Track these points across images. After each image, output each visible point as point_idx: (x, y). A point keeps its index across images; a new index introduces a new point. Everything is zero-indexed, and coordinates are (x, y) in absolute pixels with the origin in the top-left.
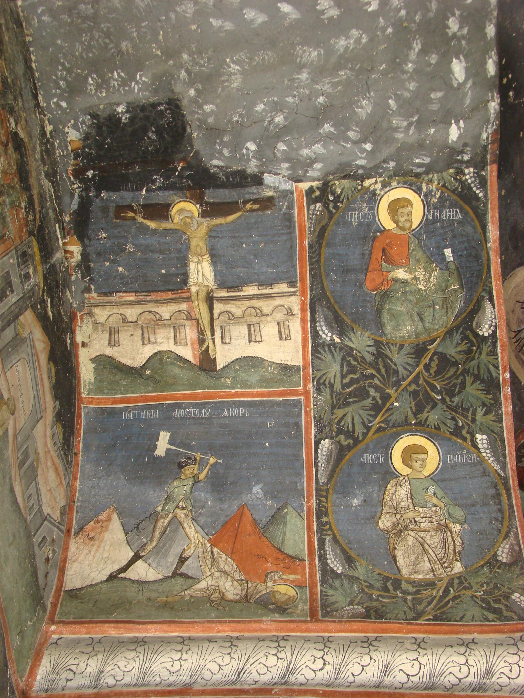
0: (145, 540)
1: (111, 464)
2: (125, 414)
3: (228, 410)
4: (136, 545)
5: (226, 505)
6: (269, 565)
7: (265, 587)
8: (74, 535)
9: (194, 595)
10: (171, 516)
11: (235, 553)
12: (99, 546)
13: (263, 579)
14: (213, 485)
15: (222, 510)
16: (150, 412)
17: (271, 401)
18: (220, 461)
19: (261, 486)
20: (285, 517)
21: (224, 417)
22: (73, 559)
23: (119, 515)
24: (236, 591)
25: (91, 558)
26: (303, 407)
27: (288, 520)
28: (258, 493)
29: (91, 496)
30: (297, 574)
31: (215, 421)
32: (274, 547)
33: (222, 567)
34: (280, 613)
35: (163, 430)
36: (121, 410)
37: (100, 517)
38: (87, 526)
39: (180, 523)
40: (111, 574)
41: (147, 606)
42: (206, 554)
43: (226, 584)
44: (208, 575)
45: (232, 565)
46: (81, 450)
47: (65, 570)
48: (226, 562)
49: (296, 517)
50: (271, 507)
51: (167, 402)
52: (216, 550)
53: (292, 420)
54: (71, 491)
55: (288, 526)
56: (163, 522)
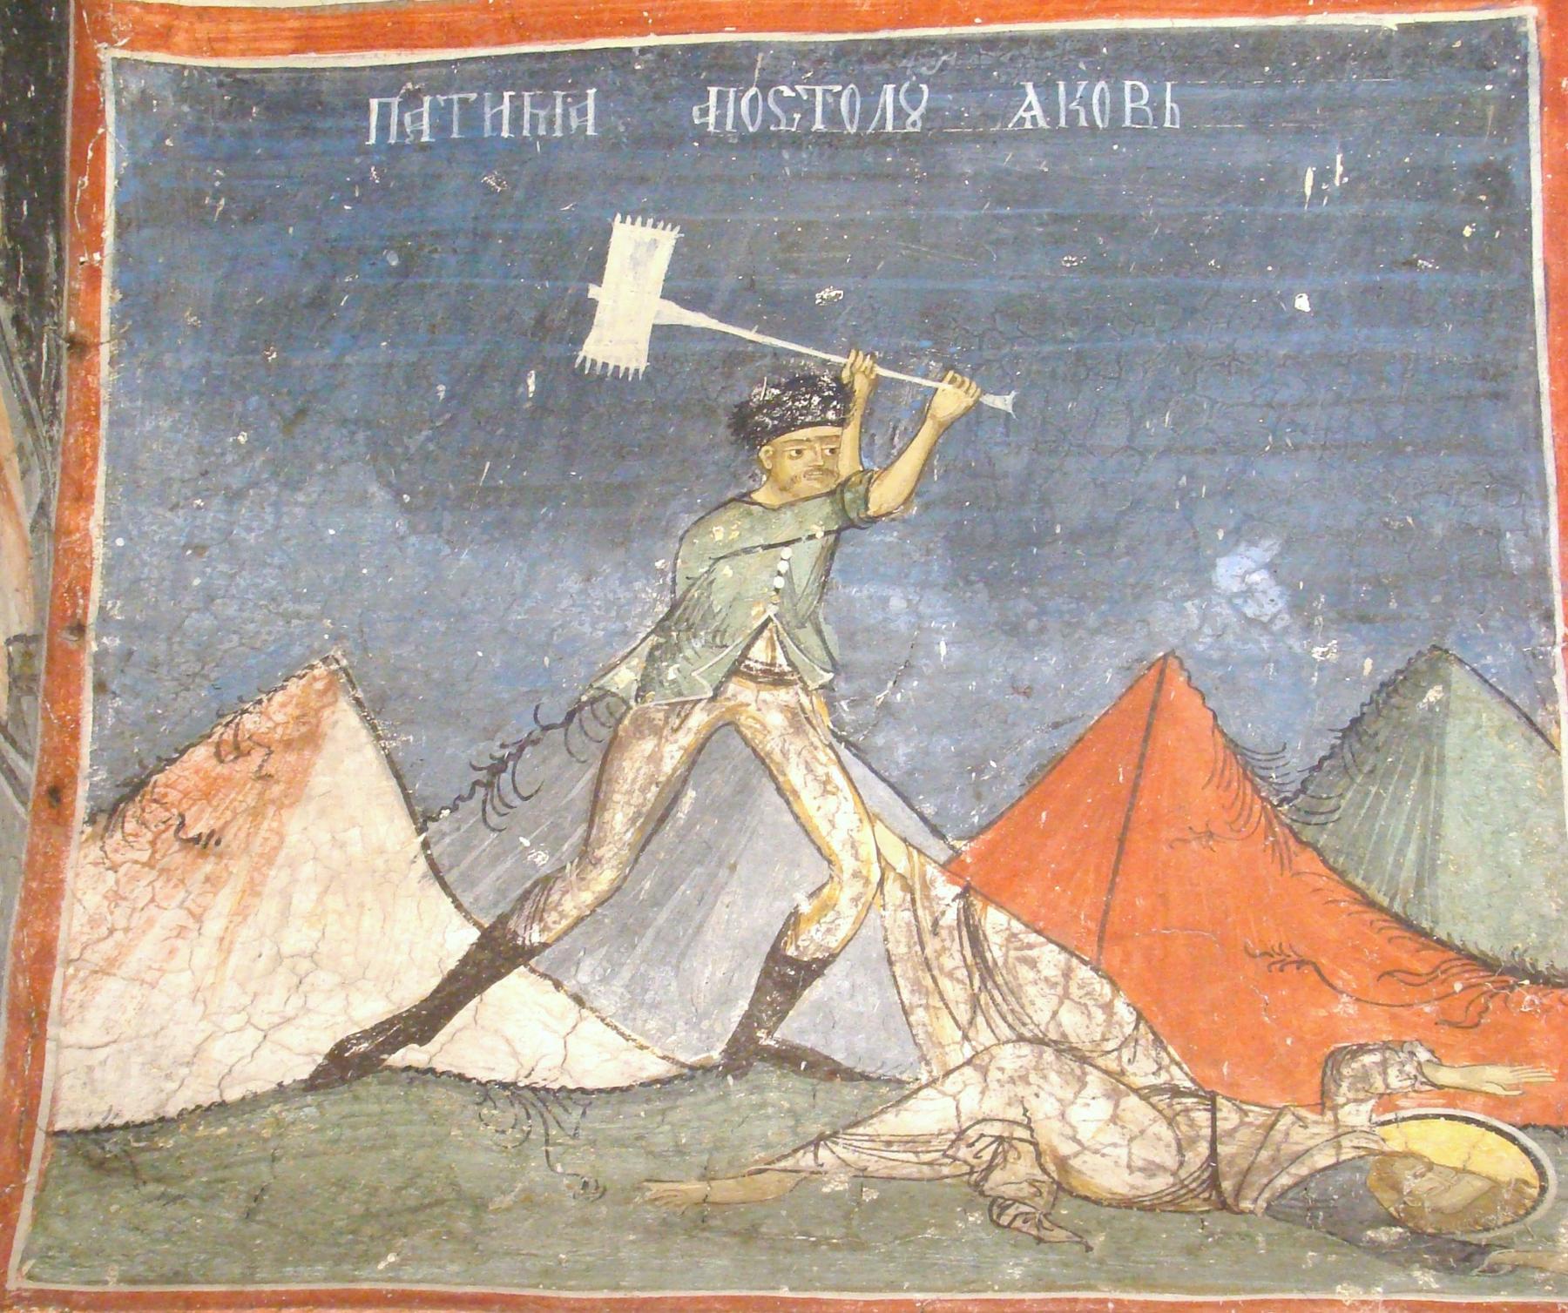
0: (541, 857)
1: (302, 412)
2: (385, 108)
3: (1046, 90)
4: (486, 886)
5: (1048, 663)
6: (1345, 1007)
7: (1326, 1131)
8: (92, 820)
9: (874, 1165)
10: (699, 718)
11: (1119, 937)
12: (253, 890)
13: (1310, 1092)
14: (960, 543)
15: (1027, 693)
16: (544, 102)
17: (1326, 37)
18: (1002, 403)
19: (1267, 549)
20: (1430, 730)
21: (1021, 136)
22: (95, 957)
23: (372, 711)
24: (1141, 1152)
25: (204, 953)
26: (1534, 71)
27: (1451, 752)
28: (1249, 593)
29: (187, 601)
30: (1530, 1058)
31: (966, 161)
32: (1371, 904)
33: (1042, 1017)
34: (1442, 1267)
35: (634, 212)
36: (356, 88)
37: (250, 722)
38: (173, 772)
39: (762, 759)
40: (341, 1047)
41: (586, 1222)
42: (932, 945)
43: (1075, 1114)
44: (955, 1058)
45: (1108, 1008)
46: (105, 325)
47: (43, 1017)
48: (1058, 987)
49: (1502, 732)
50: (1341, 673)
51: (652, 40)
52: (994, 921)
53: (1463, 153)
54: (60, 569)
55: (1452, 782)
56: (648, 761)
